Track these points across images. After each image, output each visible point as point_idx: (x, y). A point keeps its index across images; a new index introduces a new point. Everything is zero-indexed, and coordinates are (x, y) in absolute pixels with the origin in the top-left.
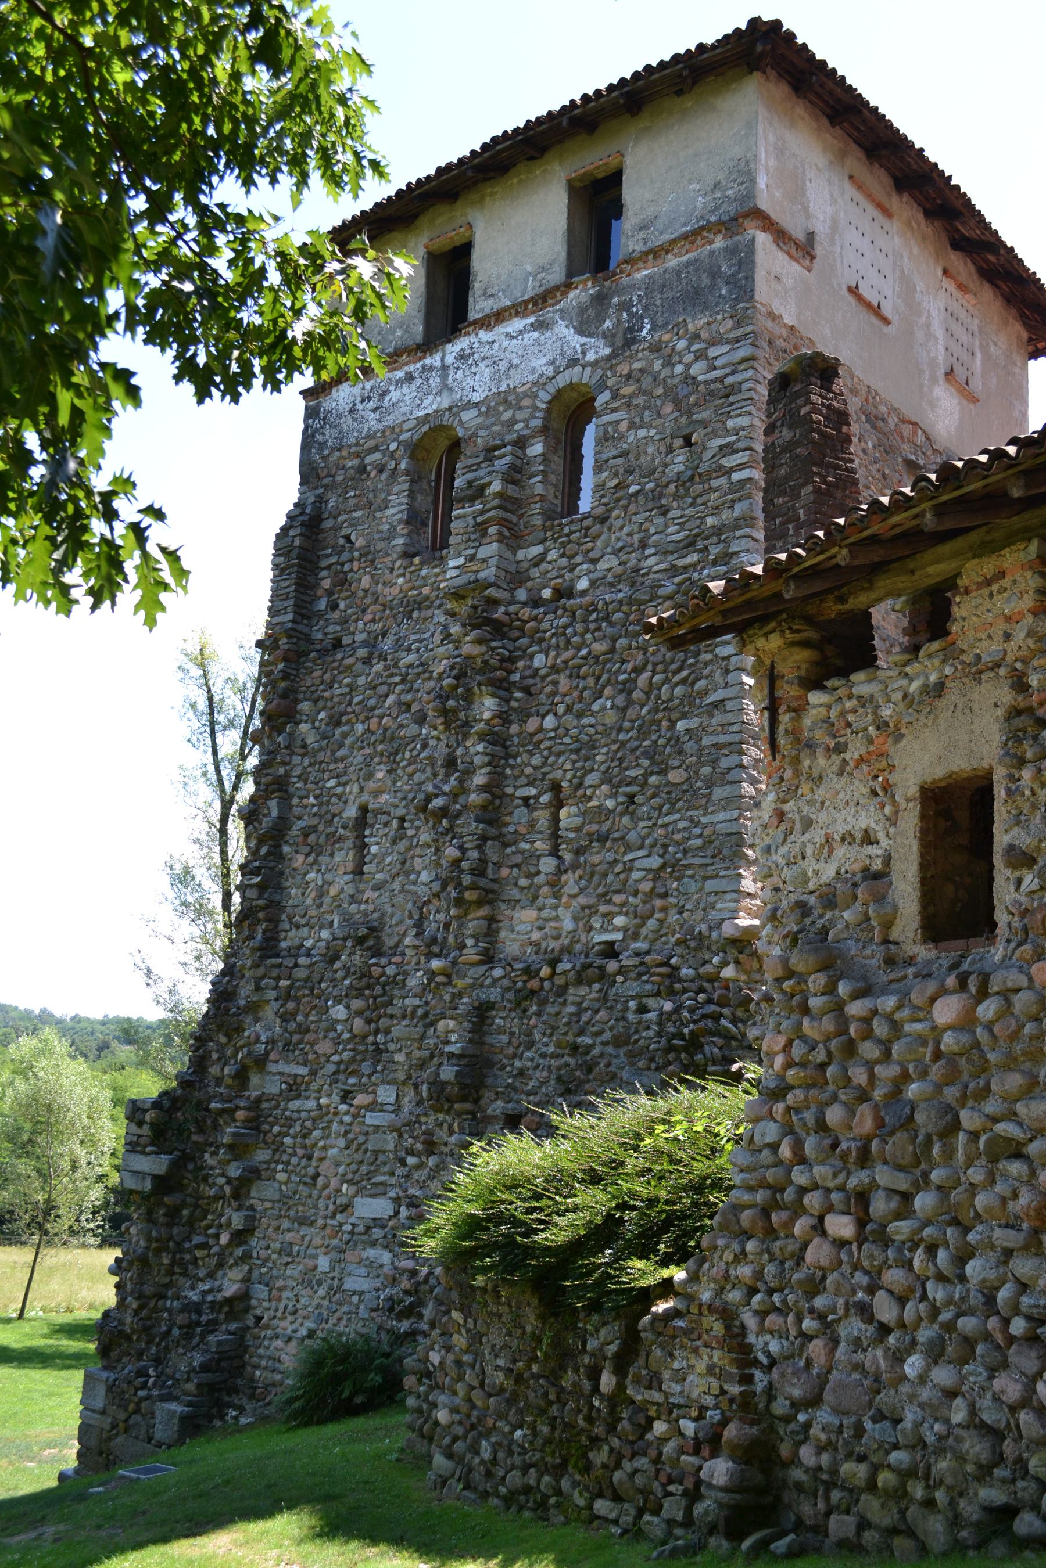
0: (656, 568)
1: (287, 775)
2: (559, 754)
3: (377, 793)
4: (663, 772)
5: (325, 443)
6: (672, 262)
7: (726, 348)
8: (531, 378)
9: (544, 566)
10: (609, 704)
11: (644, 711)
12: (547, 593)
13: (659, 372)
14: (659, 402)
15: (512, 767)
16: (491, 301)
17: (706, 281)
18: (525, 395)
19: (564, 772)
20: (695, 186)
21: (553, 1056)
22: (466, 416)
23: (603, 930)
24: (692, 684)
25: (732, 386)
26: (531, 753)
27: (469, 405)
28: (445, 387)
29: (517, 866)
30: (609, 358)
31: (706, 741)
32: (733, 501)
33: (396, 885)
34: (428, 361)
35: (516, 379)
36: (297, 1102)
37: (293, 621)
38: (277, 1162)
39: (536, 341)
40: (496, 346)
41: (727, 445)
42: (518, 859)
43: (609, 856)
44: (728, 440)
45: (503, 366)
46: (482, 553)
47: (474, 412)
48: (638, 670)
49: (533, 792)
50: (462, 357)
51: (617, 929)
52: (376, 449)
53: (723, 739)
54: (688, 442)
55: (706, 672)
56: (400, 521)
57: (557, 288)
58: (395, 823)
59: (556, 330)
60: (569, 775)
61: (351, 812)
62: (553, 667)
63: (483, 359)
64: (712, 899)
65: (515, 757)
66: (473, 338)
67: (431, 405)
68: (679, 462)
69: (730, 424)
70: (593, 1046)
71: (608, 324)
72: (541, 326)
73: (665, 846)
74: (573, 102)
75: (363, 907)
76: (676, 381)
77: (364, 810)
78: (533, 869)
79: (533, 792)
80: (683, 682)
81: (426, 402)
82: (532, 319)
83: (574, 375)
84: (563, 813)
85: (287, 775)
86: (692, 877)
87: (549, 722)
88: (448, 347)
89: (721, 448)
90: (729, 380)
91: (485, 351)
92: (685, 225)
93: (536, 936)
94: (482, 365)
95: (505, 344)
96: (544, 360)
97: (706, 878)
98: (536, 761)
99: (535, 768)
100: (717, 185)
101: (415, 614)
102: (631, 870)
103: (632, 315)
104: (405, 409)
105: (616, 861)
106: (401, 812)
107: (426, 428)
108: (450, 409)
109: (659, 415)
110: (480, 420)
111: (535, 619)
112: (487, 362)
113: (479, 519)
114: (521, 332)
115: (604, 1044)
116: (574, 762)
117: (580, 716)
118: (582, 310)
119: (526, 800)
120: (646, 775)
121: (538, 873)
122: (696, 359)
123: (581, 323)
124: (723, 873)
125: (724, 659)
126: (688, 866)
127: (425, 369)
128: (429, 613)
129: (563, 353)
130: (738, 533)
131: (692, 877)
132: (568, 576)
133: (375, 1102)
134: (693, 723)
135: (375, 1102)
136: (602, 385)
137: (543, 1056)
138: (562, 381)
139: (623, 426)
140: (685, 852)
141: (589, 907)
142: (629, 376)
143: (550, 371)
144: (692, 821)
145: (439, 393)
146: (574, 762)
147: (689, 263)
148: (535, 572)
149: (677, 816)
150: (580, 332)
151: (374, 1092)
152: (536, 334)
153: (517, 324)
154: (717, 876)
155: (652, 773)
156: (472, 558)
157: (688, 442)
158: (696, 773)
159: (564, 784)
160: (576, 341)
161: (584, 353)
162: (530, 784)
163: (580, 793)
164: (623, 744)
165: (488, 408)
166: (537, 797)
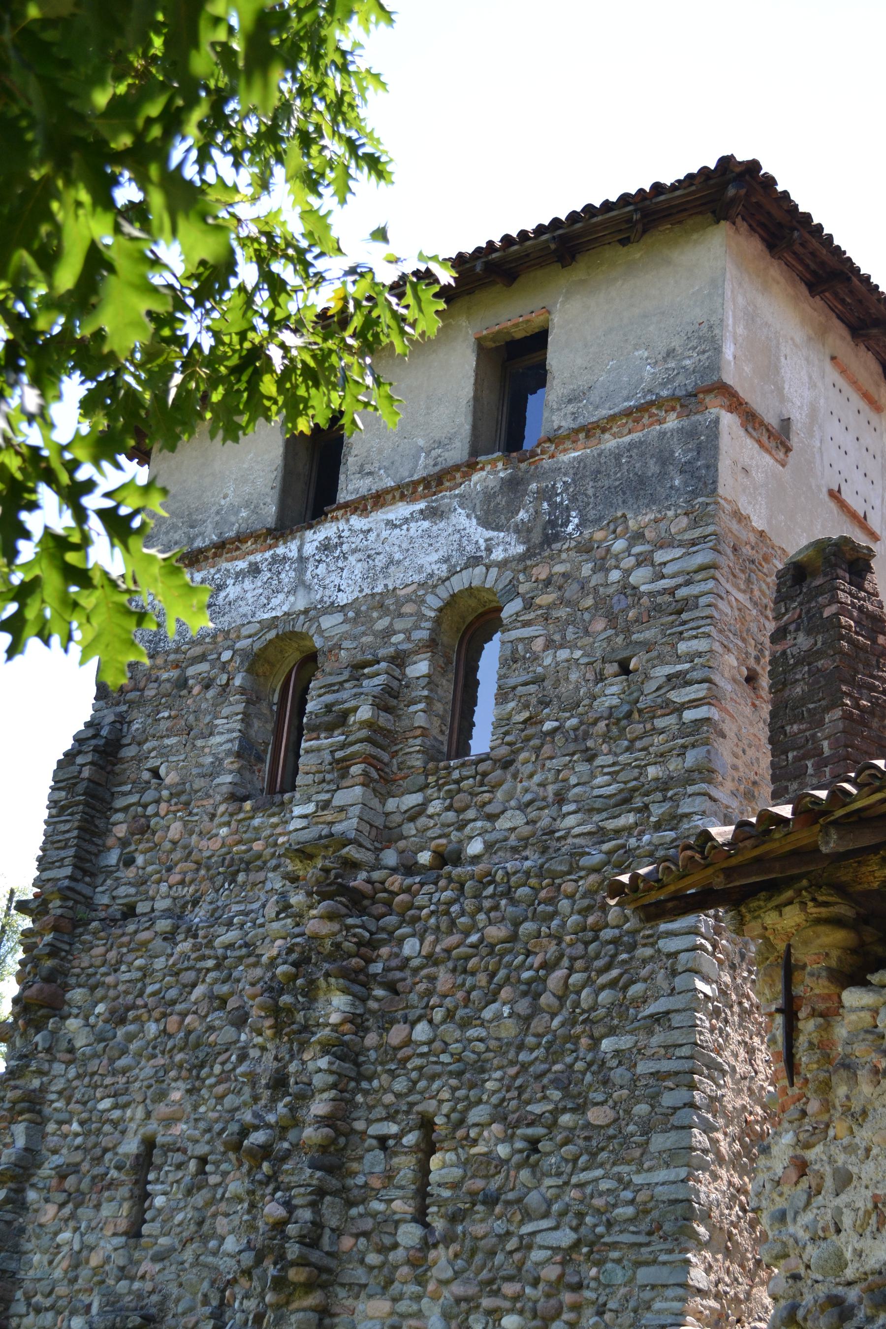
0: (577, 831)
1: (43, 1089)
2: (433, 1078)
3: (169, 1121)
4: (580, 1109)
6: (610, 443)
7: (678, 552)
8: (416, 578)
9: (422, 821)
10: (506, 1010)
11: (556, 1023)
12: (424, 858)
13: (588, 579)
14: (587, 616)
15: (366, 1093)
16: (368, 480)
17: (653, 468)
18: (408, 599)
20: (643, 353)
22: (327, 622)
24: (625, 988)
25: (686, 599)
26: (393, 1074)
27: (333, 608)
28: (301, 584)
29: (366, 1234)
30: (522, 558)
31: (643, 1068)
32: (684, 747)
33: (188, 1255)
34: (280, 550)
35: (396, 578)
37: (71, 878)
39: (427, 534)
40: (372, 536)
41: (677, 675)
42: (368, 1224)
43: (500, 1226)
44: (679, 667)
45: (381, 560)
46: (340, 798)
47: (339, 618)
48: (548, 966)
49: (394, 1129)
50: (326, 547)
52: (202, 658)
53: (666, 1066)
54: (625, 669)
55: (644, 973)
56: (229, 753)
57: (457, 468)
58: (192, 1165)
59: (453, 519)
60: (446, 1108)
61: (131, 1146)
62: (429, 957)
63: (355, 551)
64: (647, 1295)
65: (370, 1079)
66: (342, 525)
68: (612, 693)
69: (682, 647)
71: (522, 515)
72: (433, 513)
73: (580, 1215)
74: (490, 243)
76: (611, 590)
77: (149, 1144)
78: (387, 1241)
79: (394, 1129)
80: (612, 984)
81: (274, 602)
82: (422, 505)
83: (475, 576)
84: (435, 1161)
85: (43, 1089)
86: (618, 1261)
87: (422, 1031)
88: (309, 534)
89: (669, 678)
90: (682, 593)
91: (357, 541)
92: (627, 399)
94: (352, 559)
95: (385, 534)
96: (435, 557)
97: (638, 1264)
98: (400, 1085)
99: (398, 1096)
100: (670, 353)
101: (241, 877)
102: (530, 1247)
103: (554, 506)
104: (244, 609)
105: (508, 1234)
106: (201, 1149)
107: (272, 635)
108: (306, 612)
109: (587, 632)
110: (346, 627)
111: (408, 890)
112: (358, 555)
113: (339, 755)
114: (406, 521)
116: (454, 1089)
117: (465, 1024)
118: (488, 496)
119: (382, 1140)
120: (556, 1112)
121: (395, 1246)
122: (639, 564)
123: (487, 512)
124: (663, 1257)
125: (669, 955)
126: (614, 1246)
127: (275, 560)
128: (261, 876)
129: (461, 549)
130: (690, 789)
131: (618, 1261)
132: (455, 836)
134: (625, 1042)
136: (512, 591)
138: (458, 583)
140: (609, 1224)
141: (467, 1299)
142: (548, 582)
144: (620, 1180)
145: (293, 591)
146: (454, 1089)
147: (631, 446)
148: (410, 829)
149: (599, 1172)
150: (485, 523)
152: (426, 524)
153: (401, 510)
154: (655, 1262)
155: (564, 1110)
156: (325, 805)
157: (625, 669)
158: (628, 1112)
159: (439, 1120)
160: (480, 535)
161: (489, 550)
162: (390, 1117)
163: (460, 1133)
164: (525, 1067)
165: (358, 613)
166: (398, 1137)
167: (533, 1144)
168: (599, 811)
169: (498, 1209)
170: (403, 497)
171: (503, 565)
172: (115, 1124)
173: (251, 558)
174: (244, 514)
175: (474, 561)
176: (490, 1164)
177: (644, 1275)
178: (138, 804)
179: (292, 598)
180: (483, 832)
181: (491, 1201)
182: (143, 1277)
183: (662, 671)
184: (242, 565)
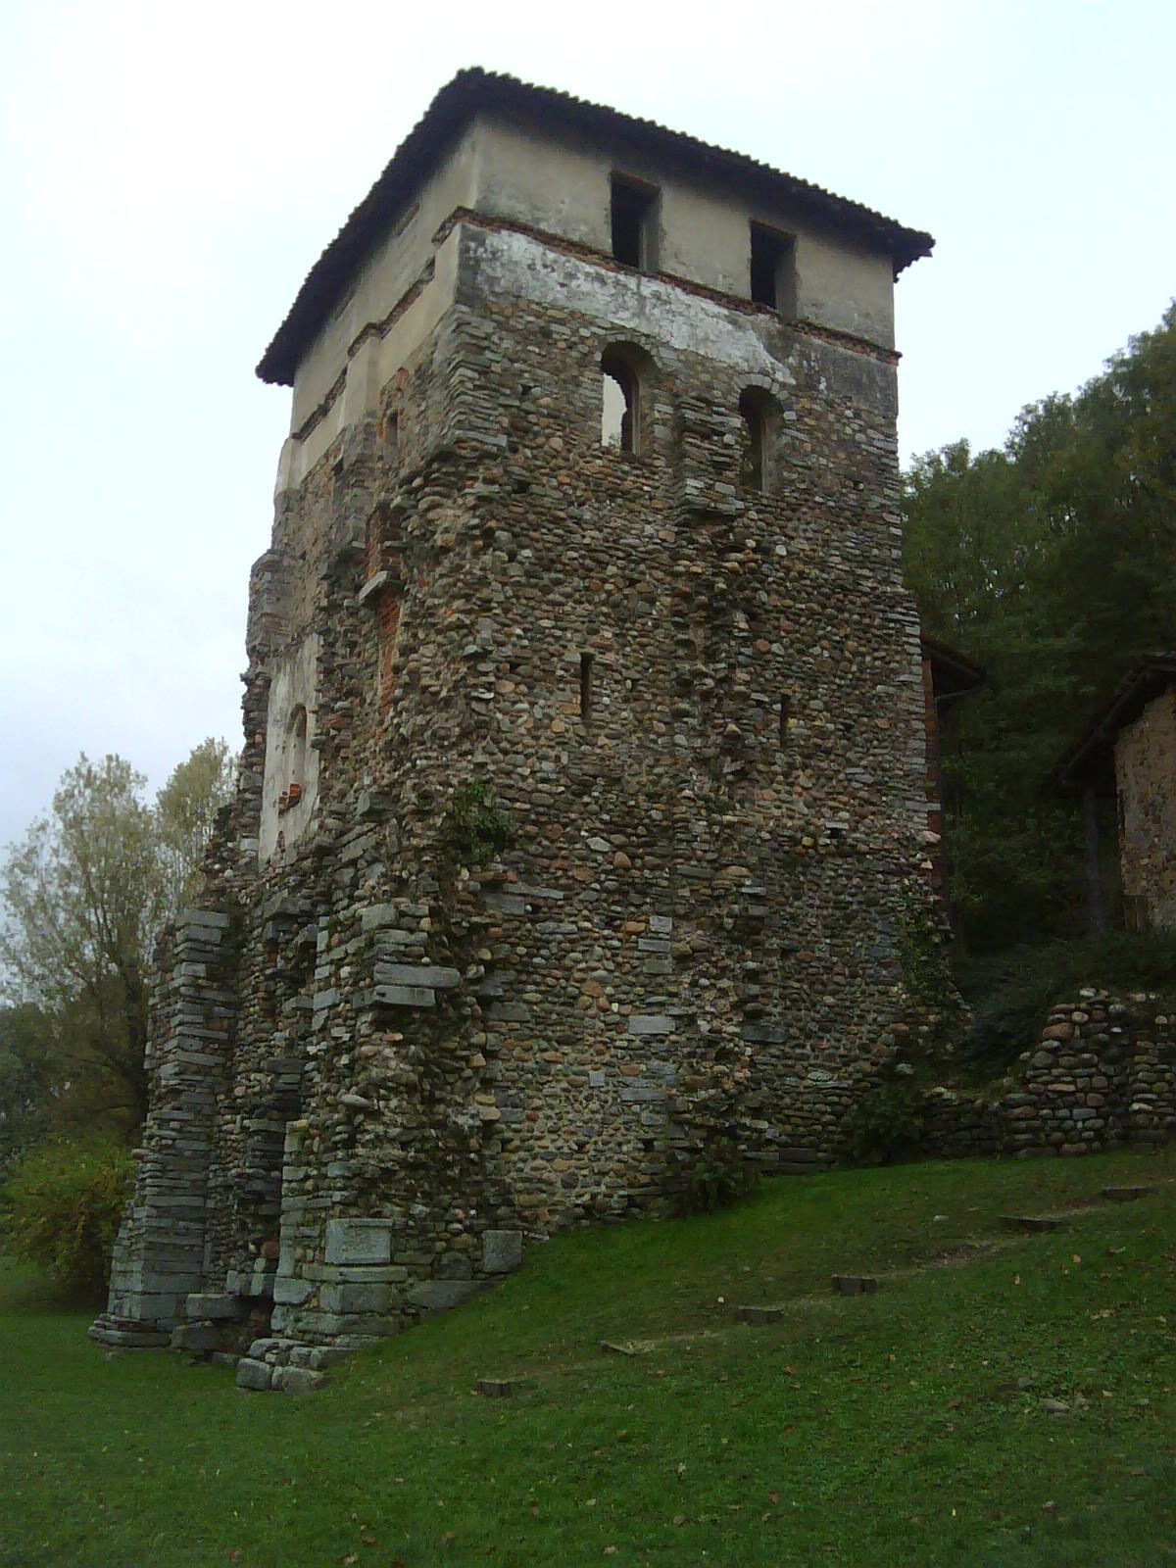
2: (787, 677)
3: (604, 649)
5: (497, 279)
19: (795, 690)
21: (819, 907)
23: (831, 820)
27: (666, 345)
36: (551, 925)
38: (524, 983)
40: (692, 312)
45: (700, 334)
51: (841, 821)
67: (625, 319)
70: (851, 903)
75: (598, 751)
77: (587, 659)
81: (621, 314)
82: (726, 312)
87: (775, 647)
90: (885, 460)
93: (777, 812)
94: (680, 319)
96: (739, 354)
97: (905, 799)
100: (867, 315)
102: (850, 780)
107: (622, 338)
113: (716, 458)
115: (860, 903)
117: (801, 652)
119: (760, 703)
126: (894, 788)
127: (617, 283)
133: (647, 930)
135: (647, 930)
137: (811, 906)
139: (808, 447)
143: (745, 366)
150: (771, 349)
151: (647, 922)
152: (730, 327)
153: (710, 306)
160: (767, 359)
162: (764, 691)
164: (840, 686)
167: (848, 728)
168: (850, 561)
169: (832, 757)
170: (712, 298)
171: (783, 385)
172: (558, 639)
173: (598, 269)
174: (583, 228)
175: (764, 373)
176: (823, 733)
177: (908, 803)
178: (518, 407)
179: (637, 320)
180: (784, 544)
181: (828, 752)
182: (601, 747)
183: (878, 500)
184: (588, 269)
